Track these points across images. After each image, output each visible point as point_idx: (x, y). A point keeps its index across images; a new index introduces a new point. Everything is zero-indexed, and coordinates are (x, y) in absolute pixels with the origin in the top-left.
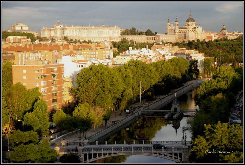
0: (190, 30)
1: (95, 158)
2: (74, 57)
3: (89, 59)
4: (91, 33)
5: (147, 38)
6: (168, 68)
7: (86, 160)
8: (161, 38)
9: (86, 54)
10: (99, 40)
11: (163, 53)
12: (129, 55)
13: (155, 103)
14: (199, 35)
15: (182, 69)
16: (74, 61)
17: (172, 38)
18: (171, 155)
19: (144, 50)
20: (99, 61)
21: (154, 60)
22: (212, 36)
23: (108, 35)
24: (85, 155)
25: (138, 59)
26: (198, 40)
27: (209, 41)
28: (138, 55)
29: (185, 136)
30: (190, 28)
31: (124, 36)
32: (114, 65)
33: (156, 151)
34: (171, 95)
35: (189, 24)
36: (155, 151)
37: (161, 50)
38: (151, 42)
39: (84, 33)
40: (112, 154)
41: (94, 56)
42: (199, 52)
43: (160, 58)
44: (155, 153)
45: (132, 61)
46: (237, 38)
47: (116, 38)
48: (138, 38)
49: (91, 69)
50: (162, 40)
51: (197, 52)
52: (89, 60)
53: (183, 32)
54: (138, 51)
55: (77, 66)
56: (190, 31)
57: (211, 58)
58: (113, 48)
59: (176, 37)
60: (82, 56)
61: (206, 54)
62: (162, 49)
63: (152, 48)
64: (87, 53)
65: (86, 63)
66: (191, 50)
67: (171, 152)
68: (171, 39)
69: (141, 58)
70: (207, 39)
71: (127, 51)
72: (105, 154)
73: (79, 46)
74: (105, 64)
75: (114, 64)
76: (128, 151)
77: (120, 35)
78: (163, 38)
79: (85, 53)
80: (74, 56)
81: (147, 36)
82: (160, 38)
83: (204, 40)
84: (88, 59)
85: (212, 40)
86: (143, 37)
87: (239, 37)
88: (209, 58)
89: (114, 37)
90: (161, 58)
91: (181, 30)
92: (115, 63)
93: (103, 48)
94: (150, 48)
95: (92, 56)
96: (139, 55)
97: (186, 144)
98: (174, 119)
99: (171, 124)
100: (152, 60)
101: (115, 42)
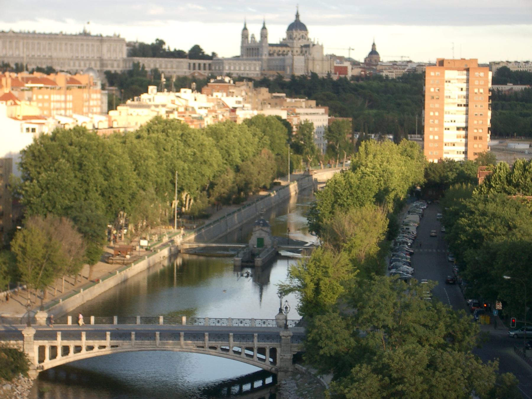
0: (295, 50)
1: (65, 357)
2: (14, 107)
3: (50, 113)
4: (55, 49)
5: (192, 65)
6: (244, 141)
7: (43, 361)
8: (227, 68)
9: (43, 101)
10: (74, 65)
11: (231, 102)
12: (148, 107)
13: (210, 224)
14: (316, 63)
15: (278, 144)
16: (14, 116)
17: (253, 68)
18: (251, 353)
19: (186, 93)
20: (74, 119)
21: (209, 121)
22: (346, 68)
23: (96, 55)
24: (42, 349)
25: (172, 116)
26: (314, 75)
27: (340, 79)
28: (170, 106)
29: (286, 308)
30: (295, 45)
31: (136, 59)
32: (112, 130)
33: (214, 342)
34: (249, 205)
35: (294, 36)
36: (213, 343)
37: (227, 96)
38: (201, 75)
39: (39, 49)
40: (107, 349)
41: (63, 105)
42: (317, 105)
43: (223, 116)
44: (104, 347)
45: (158, 120)
47: (115, 64)
48: (169, 66)
49: (54, 137)
50: (228, 72)
51: (313, 103)
52: (50, 115)
54: (172, 95)
55: (22, 129)
56: (295, 53)
57: (345, 119)
58: (107, 88)
59: (262, 66)
60: (34, 104)
61: (333, 111)
62: (230, 94)
63: (205, 89)
64: (46, 97)
65: (43, 124)
66: (298, 100)
67: (250, 344)
68: (250, 70)
69: (179, 113)
70: (335, 74)
71: (144, 96)
72: (90, 348)
73: (27, 80)
74: (89, 127)
75: (112, 127)
76: (147, 342)
77: (125, 56)
78: (230, 69)
79: (40, 97)
80: (15, 104)
81: (192, 61)
82: (223, 67)
83: (329, 75)
84: (46, 113)
85: (346, 78)
86: (182, 62)
87: (407, 73)
88: (340, 119)
89: (112, 60)
90: (227, 114)
92: (115, 125)
93: (85, 87)
94: (199, 90)
95: (58, 105)
96: (174, 106)
97: (286, 326)
98: (256, 264)
99: (250, 278)
100: (206, 119)
101: (113, 72)
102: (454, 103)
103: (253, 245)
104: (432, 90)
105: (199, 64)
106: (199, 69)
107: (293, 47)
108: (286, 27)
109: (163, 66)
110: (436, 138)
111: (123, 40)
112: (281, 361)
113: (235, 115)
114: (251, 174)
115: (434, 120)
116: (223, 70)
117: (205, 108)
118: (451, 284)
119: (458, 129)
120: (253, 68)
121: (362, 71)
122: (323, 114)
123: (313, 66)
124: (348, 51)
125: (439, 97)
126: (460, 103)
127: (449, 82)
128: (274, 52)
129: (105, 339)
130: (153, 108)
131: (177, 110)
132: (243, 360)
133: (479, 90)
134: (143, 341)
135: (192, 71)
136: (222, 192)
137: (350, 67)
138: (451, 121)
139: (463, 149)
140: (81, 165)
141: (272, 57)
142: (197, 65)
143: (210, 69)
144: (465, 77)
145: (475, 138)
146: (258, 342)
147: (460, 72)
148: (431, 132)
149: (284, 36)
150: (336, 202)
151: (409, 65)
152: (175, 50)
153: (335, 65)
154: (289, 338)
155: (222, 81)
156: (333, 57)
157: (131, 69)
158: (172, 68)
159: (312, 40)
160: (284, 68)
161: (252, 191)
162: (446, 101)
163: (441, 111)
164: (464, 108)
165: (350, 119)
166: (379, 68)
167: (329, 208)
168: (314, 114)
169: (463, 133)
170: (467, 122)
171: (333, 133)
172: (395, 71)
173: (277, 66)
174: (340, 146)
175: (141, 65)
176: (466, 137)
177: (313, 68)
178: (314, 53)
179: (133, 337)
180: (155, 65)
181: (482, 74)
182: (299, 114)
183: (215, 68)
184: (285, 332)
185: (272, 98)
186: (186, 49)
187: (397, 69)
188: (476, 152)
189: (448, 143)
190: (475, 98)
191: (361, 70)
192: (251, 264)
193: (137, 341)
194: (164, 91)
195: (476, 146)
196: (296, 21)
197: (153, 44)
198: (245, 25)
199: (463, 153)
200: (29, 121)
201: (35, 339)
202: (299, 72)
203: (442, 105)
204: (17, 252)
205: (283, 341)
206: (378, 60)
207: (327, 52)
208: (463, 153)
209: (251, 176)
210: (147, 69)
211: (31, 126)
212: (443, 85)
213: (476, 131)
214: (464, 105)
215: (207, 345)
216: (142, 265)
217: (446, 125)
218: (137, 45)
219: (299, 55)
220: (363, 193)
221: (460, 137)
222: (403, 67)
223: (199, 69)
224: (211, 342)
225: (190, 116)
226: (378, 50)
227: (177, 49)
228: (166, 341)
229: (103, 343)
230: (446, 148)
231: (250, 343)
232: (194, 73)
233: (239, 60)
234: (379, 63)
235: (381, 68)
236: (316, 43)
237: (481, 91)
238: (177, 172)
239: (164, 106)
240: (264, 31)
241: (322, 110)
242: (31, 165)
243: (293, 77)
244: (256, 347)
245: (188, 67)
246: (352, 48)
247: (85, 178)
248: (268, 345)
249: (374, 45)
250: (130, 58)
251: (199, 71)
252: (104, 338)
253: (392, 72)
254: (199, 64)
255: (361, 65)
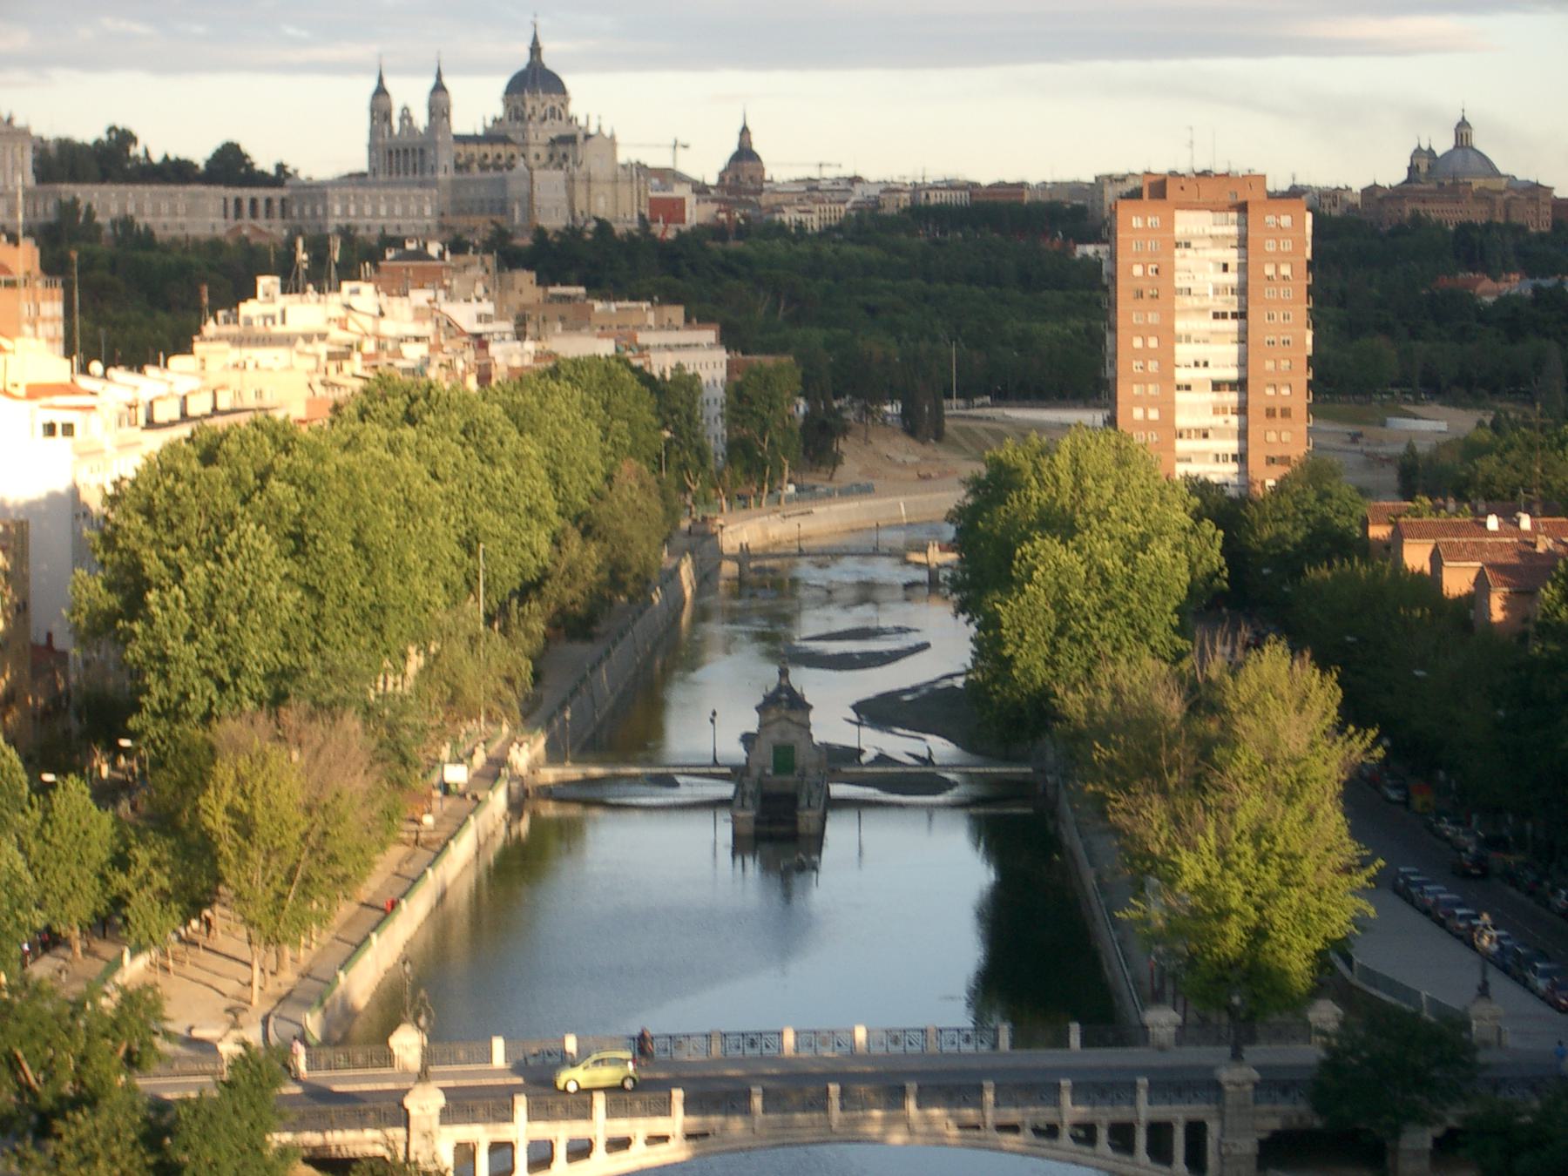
0: (533, 151)
8: (337, 210)
14: (595, 189)
17: (413, 208)
22: (682, 201)
30: (532, 137)
31: (67, 190)
35: (528, 111)
38: (260, 232)
40: (672, 1143)
42: (688, 320)
44: (664, 1139)
46: (848, 216)
48: (165, 208)
50: (343, 222)
51: (676, 313)
53: (484, 168)
65: (92, 408)
71: (247, 309)
81: (232, 193)
82: (325, 209)
86: (203, 195)
91: (473, 149)
102: (1204, 310)
103: (763, 768)
104: (1138, 270)
105: (254, 202)
106: (254, 214)
107: (527, 144)
108: (502, 83)
109: (148, 208)
110: (1154, 415)
111: (24, 133)
112: (1222, 1163)
113: (488, 357)
114: (627, 541)
115: (1146, 364)
116: (325, 215)
117: (417, 339)
118: (1475, 877)
119: (1217, 386)
120: (413, 208)
121: (719, 211)
122: (711, 346)
123: (589, 198)
124: (672, 150)
125: (1162, 292)
126: (1220, 310)
127: (1188, 245)
128: (470, 160)
129: (669, 1114)
130: (300, 344)
131: (359, 349)
132: (1101, 1162)
133: (1277, 268)
134: (787, 1116)
135: (232, 223)
136: (568, 600)
137: (691, 200)
138: (1196, 364)
139: (1232, 446)
140: (298, 538)
141: (465, 176)
142: (246, 205)
143: (285, 212)
144: (1233, 230)
145: (1270, 413)
146: (1150, 1103)
147: (1220, 216)
148: (1138, 396)
149: (498, 110)
150: (1060, 632)
151: (858, 188)
152: (166, 158)
153: (652, 194)
154: (1249, 1087)
155: (421, 254)
156: (641, 170)
157: (52, 219)
158: (174, 213)
159: (582, 122)
160: (503, 208)
161: (624, 592)
162: (1182, 302)
163: (1169, 337)
164: (1232, 325)
165: (787, 360)
166: (764, 200)
167: (1044, 650)
168: (687, 346)
169: (1232, 398)
170: (1243, 363)
171: (752, 403)
172: (817, 208)
173: (482, 201)
174: (771, 442)
175: (82, 206)
176: (1242, 410)
177: (589, 204)
178: (592, 161)
179: (757, 1102)
180: (123, 207)
181: (1286, 221)
182: (647, 347)
183: (301, 210)
184: (1237, 1070)
185: (550, 302)
186: (199, 153)
187: (822, 202)
188: (1272, 454)
189: (1189, 431)
190: (1269, 293)
191: (715, 207)
192: (783, 829)
193: (771, 1117)
194: (305, 291)
195: (1272, 437)
196: (530, 65)
197: (98, 143)
198: (381, 80)
199: (1234, 458)
200: (46, 401)
201: (442, 1122)
202: (553, 220)
203: (1169, 315)
204: (218, 827)
205: (1229, 1100)
206: (758, 184)
207: (623, 156)
208: (1234, 458)
209: (625, 547)
210: (99, 219)
211: (59, 419)
212: (1172, 256)
213: (1270, 392)
214: (1234, 316)
215: (989, 1122)
216: (462, 849)
217: (1182, 375)
218: (52, 147)
219: (545, 167)
220: (1145, 599)
221: (1225, 411)
222: (837, 196)
223: (254, 214)
224: (1003, 1110)
225: (390, 365)
226: (757, 147)
227: (172, 157)
228: (860, 1113)
229: (659, 1125)
230: (1182, 446)
231: (1126, 1108)
232: (239, 228)
233: (362, 185)
234: (765, 186)
235: (773, 200)
236: (593, 130)
237: (1285, 270)
238: (482, 546)
239: (323, 337)
240: (440, 97)
241: (709, 335)
242: (141, 538)
243: (540, 232)
244: (1143, 1119)
245: (222, 212)
246: (682, 140)
247: (315, 580)
248: (1178, 1113)
249: (745, 131)
250: (47, 187)
251: (252, 222)
252: (664, 1110)
253: (809, 212)
254: (254, 202)
255: (712, 192)
